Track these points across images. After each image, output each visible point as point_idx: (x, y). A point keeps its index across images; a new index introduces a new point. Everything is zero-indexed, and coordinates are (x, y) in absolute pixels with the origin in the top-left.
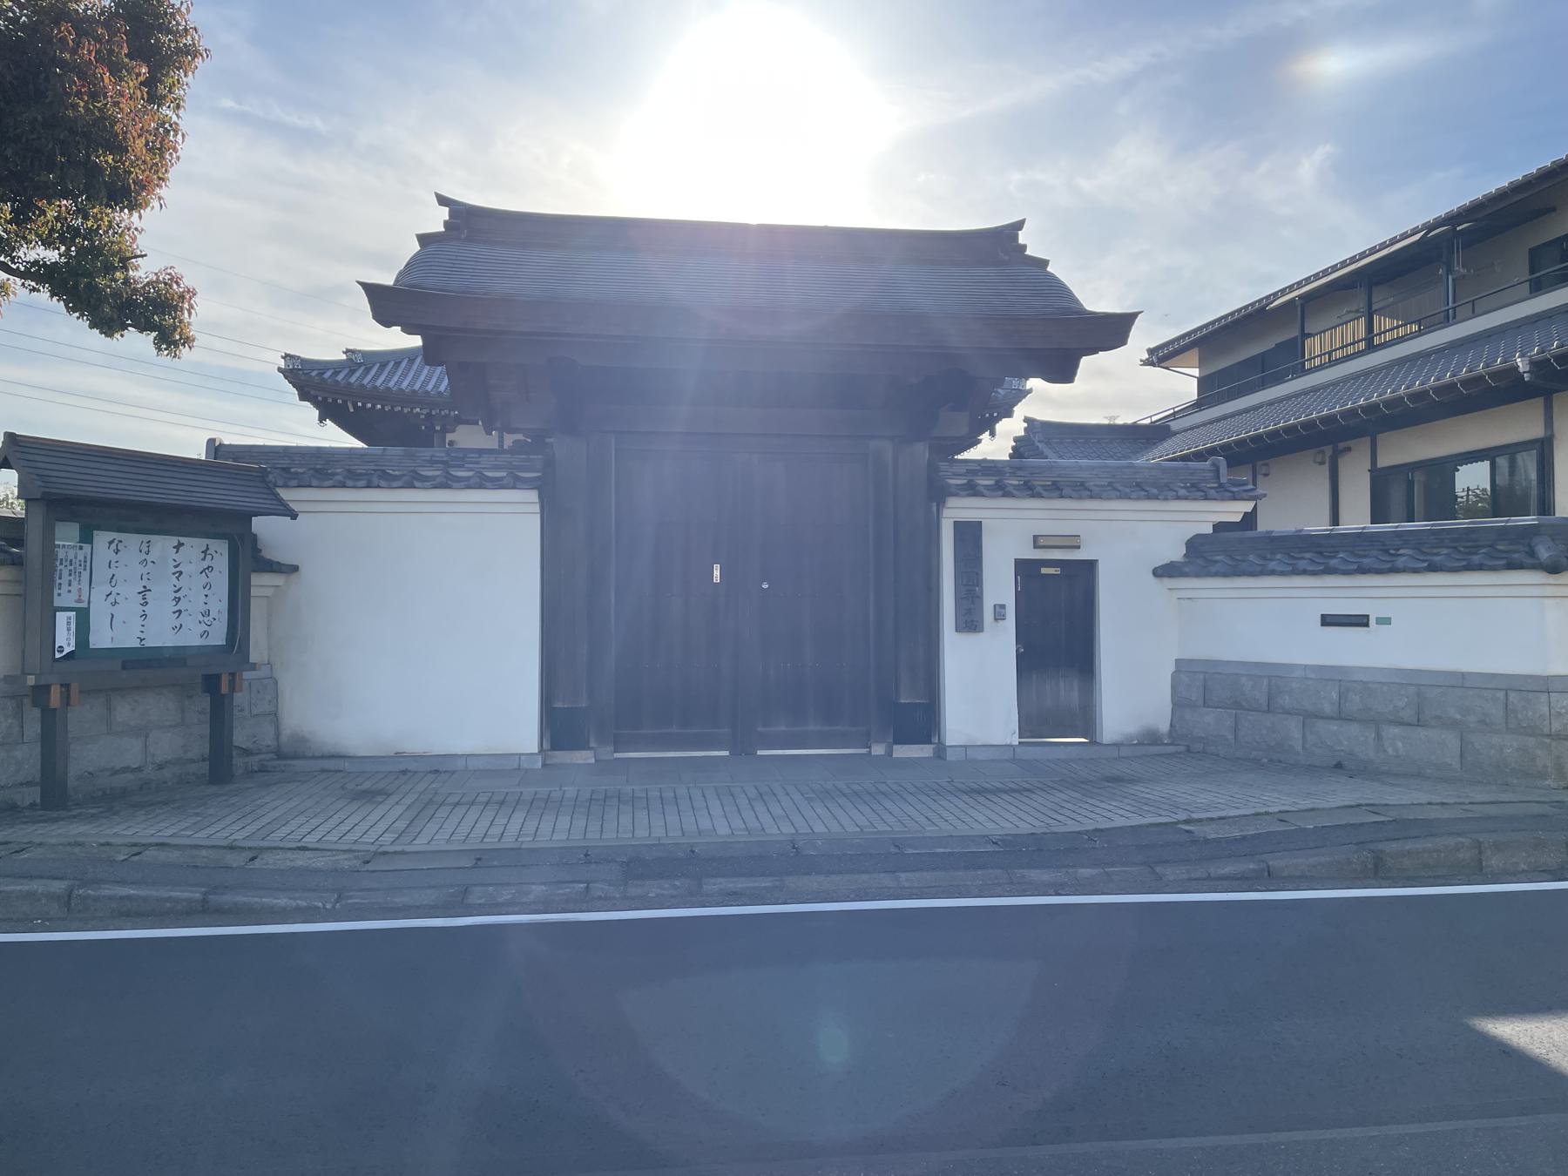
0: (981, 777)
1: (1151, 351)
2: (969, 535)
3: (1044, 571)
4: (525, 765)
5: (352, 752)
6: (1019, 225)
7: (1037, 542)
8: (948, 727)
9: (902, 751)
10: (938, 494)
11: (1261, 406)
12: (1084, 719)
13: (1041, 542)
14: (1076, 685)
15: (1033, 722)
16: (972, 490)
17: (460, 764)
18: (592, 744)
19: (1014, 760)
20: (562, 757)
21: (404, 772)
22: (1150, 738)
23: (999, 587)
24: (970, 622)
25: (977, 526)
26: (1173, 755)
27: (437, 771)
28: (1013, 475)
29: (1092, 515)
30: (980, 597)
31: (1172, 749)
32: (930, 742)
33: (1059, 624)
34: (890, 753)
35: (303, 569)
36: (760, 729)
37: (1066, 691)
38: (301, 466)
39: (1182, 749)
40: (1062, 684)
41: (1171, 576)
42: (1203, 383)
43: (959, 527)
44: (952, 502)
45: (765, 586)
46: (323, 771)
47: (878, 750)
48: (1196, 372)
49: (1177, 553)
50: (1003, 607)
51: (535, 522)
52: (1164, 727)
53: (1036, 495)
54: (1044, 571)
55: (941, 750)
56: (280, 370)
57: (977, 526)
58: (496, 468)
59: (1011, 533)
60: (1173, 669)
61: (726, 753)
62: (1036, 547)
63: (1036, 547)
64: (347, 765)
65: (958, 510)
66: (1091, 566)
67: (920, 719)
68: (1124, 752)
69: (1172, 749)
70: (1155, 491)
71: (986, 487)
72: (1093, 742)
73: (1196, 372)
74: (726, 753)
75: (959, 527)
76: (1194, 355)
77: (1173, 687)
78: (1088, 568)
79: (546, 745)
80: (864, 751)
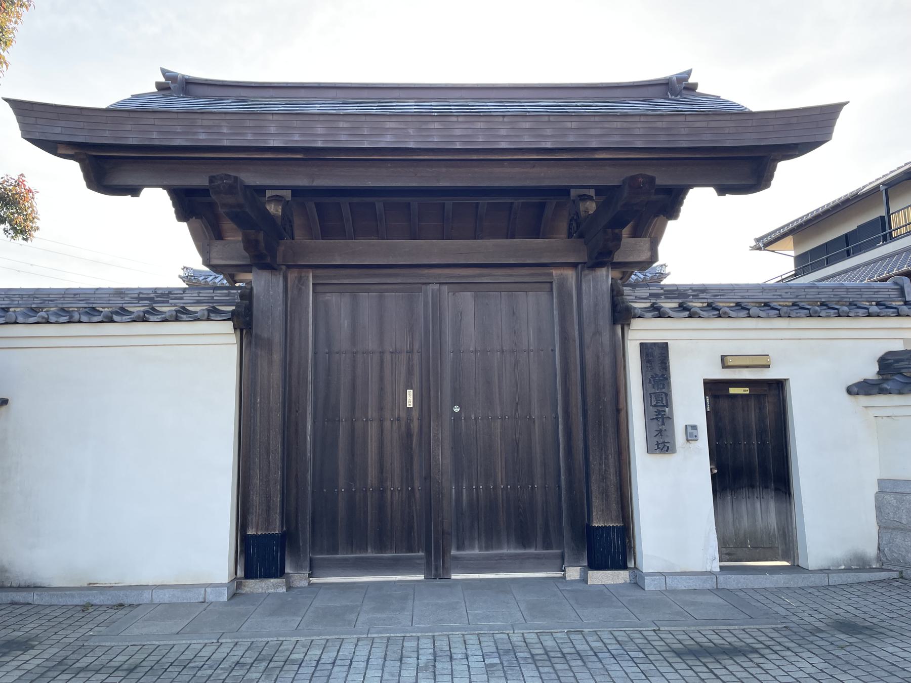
0: (679, 595)
1: (758, 240)
2: (656, 358)
3: (733, 391)
4: (211, 598)
5: (39, 581)
6: (689, 73)
7: (725, 363)
8: (644, 552)
9: (599, 578)
10: (621, 315)
11: (858, 267)
12: (785, 542)
13: (730, 361)
14: (772, 505)
15: (733, 547)
16: (660, 313)
17: (146, 596)
18: (288, 570)
19: (717, 591)
20: (255, 586)
21: (85, 608)
22: (859, 564)
23: (690, 408)
24: (661, 443)
25: (664, 347)
26: (887, 582)
27: (121, 605)
28: (696, 297)
29: (772, 334)
30: (670, 418)
31: (883, 575)
32: (624, 567)
33: (752, 447)
34: (584, 580)
35: (10, 401)
36: (454, 552)
37: (760, 512)
38: (18, 306)
39: (895, 575)
40: (758, 505)
41: (867, 394)
42: (799, 259)
43: (645, 348)
44: (636, 323)
45: (456, 409)
46: (13, 603)
47: (573, 573)
48: (792, 253)
49: (871, 371)
50: (694, 427)
51: (234, 351)
52: (871, 550)
53: (720, 314)
54: (733, 391)
55: (637, 582)
56: (180, 277)
57: (664, 347)
58: (198, 302)
59: (698, 356)
60: (876, 489)
61: (422, 577)
62: (724, 366)
63: (724, 366)
64: (34, 598)
65: (642, 332)
66: (779, 385)
67: (612, 547)
68: (835, 579)
69: (883, 575)
70: (846, 308)
71: (673, 309)
72: (796, 568)
73: (792, 253)
74: (422, 577)
75: (645, 348)
76: (789, 240)
77: (879, 509)
78: (777, 388)
79: (241, 573)
80: (559, 574)
